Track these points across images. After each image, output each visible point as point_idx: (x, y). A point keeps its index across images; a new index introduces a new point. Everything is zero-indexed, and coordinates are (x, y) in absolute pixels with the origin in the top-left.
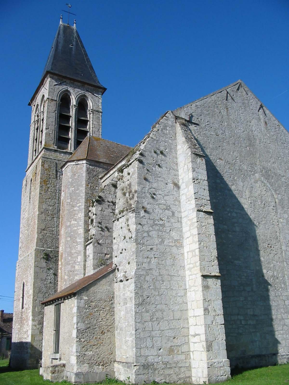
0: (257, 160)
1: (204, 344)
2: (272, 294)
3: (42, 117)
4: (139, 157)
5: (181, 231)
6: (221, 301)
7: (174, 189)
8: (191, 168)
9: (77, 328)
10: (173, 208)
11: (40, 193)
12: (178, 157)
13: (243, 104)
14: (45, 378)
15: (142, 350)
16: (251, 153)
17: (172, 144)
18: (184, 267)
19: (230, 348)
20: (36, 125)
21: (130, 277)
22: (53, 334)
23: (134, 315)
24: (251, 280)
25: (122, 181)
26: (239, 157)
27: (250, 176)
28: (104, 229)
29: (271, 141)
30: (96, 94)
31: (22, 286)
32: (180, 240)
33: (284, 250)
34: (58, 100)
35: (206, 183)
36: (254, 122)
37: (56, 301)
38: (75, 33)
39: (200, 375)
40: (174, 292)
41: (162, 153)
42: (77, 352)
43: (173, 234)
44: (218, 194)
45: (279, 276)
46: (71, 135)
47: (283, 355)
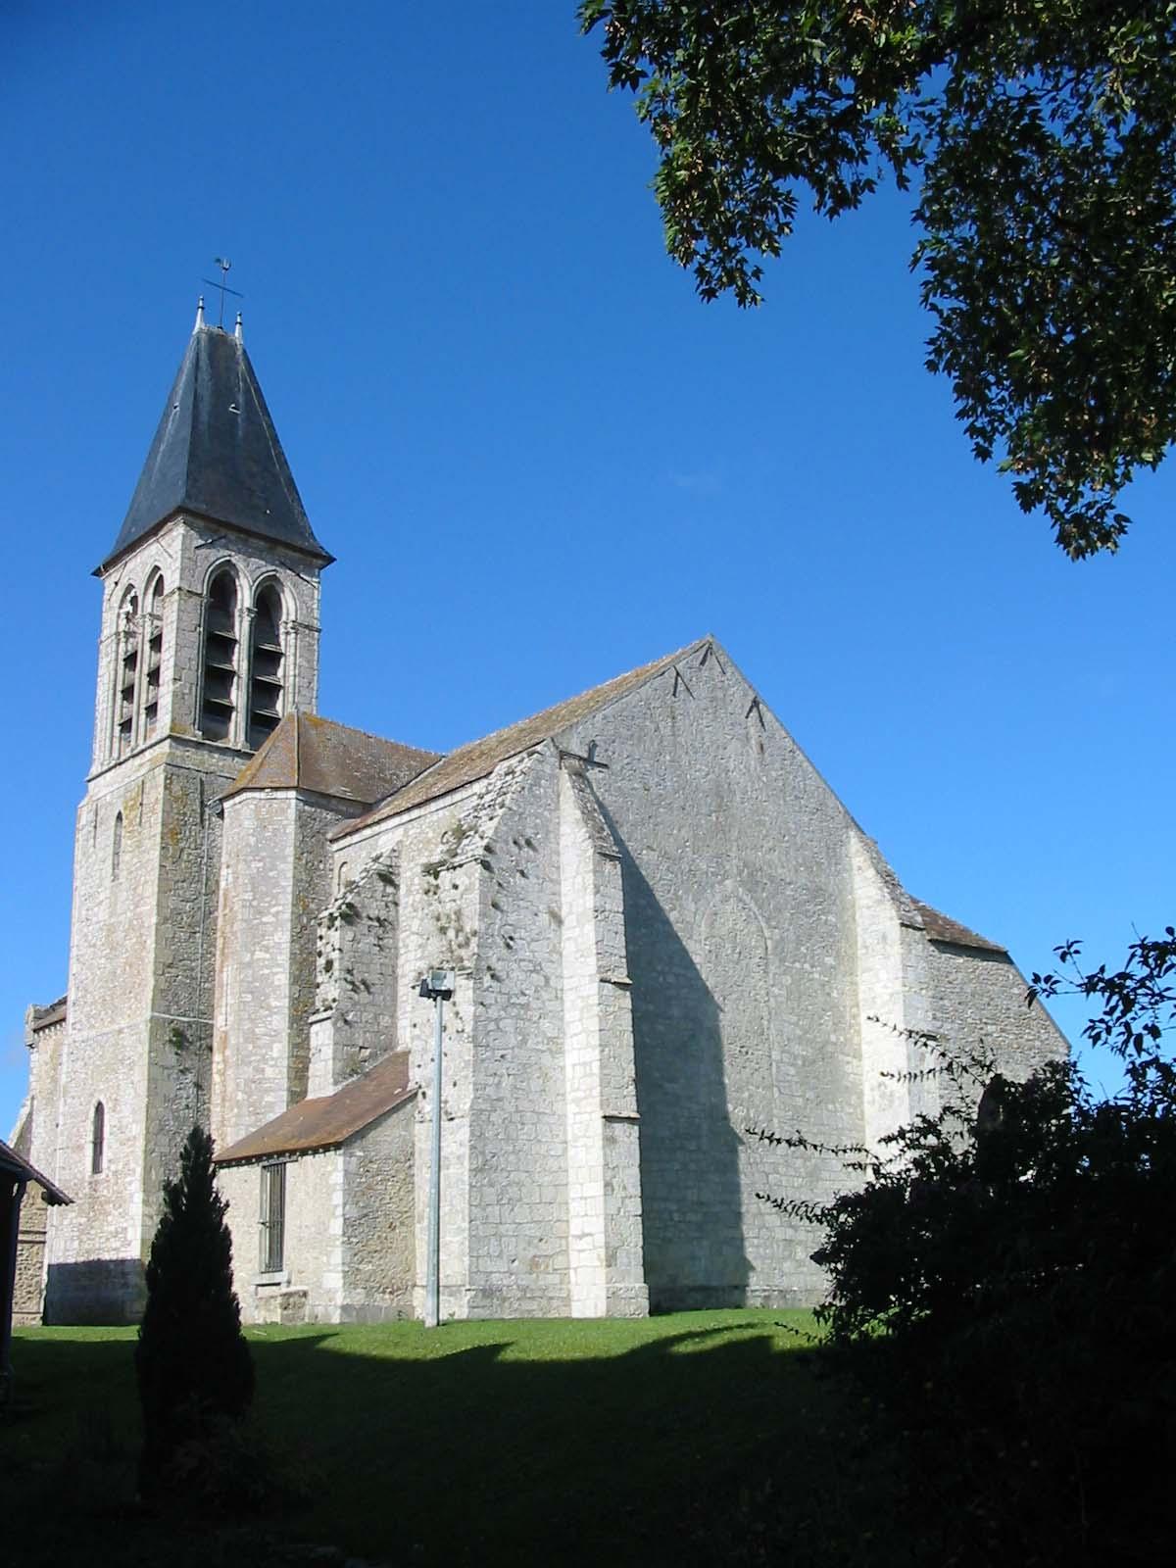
1: (602, 1252)
5: (562, 1019)
9: (344, 1215)
10: (548, 969)
12: (562, 851)
18: (563, 1095)
19: (650, 1269)
20: (122, 645)
21: (459, 1114)
27: (712, 886)
36: (734, 746)
38: (240, 361)
40: (544, 1147)
41: (529, 843)
42: (343, 1264)
43: (545, 1024)
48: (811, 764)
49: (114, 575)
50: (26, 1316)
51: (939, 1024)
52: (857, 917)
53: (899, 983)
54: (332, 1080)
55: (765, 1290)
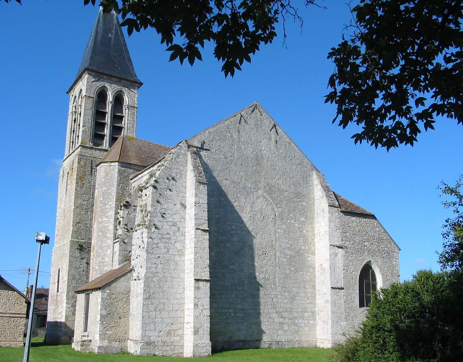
0: (262, 177)
1: (193, 329)
2: (262, 292)
3: (79, 110)
4: (154, 184)
5: (184, 243)
6: (209, 299)
7: (181, 208)
9: (101, 314)
10: (179, 225)
11: (76, 189)
12: (187, 181)
14: (76, 350)
15: (147, 332)
17: (183, 170)
18: (184, 271)
20: (74, 116)
22: (83, 317)
23: (142, 306)
24: (243, 281)
28: (129, 230)
30: (133, 89)
31: (58, 271)
32: (182, 250)
33: (278, 256)
37: (86, 292)
38: (115, 19)
39: (189, 352)
41: (173, 179)
45: (270, 278)
46: (107, 131)
47: (265, 342)
48: (298, 147)
49: (72, 93)
50: (18, 342)
51: (344, 242)
52: (315, 203)
53: (328, 227)
54: (118, 263)
55: (269, 341)
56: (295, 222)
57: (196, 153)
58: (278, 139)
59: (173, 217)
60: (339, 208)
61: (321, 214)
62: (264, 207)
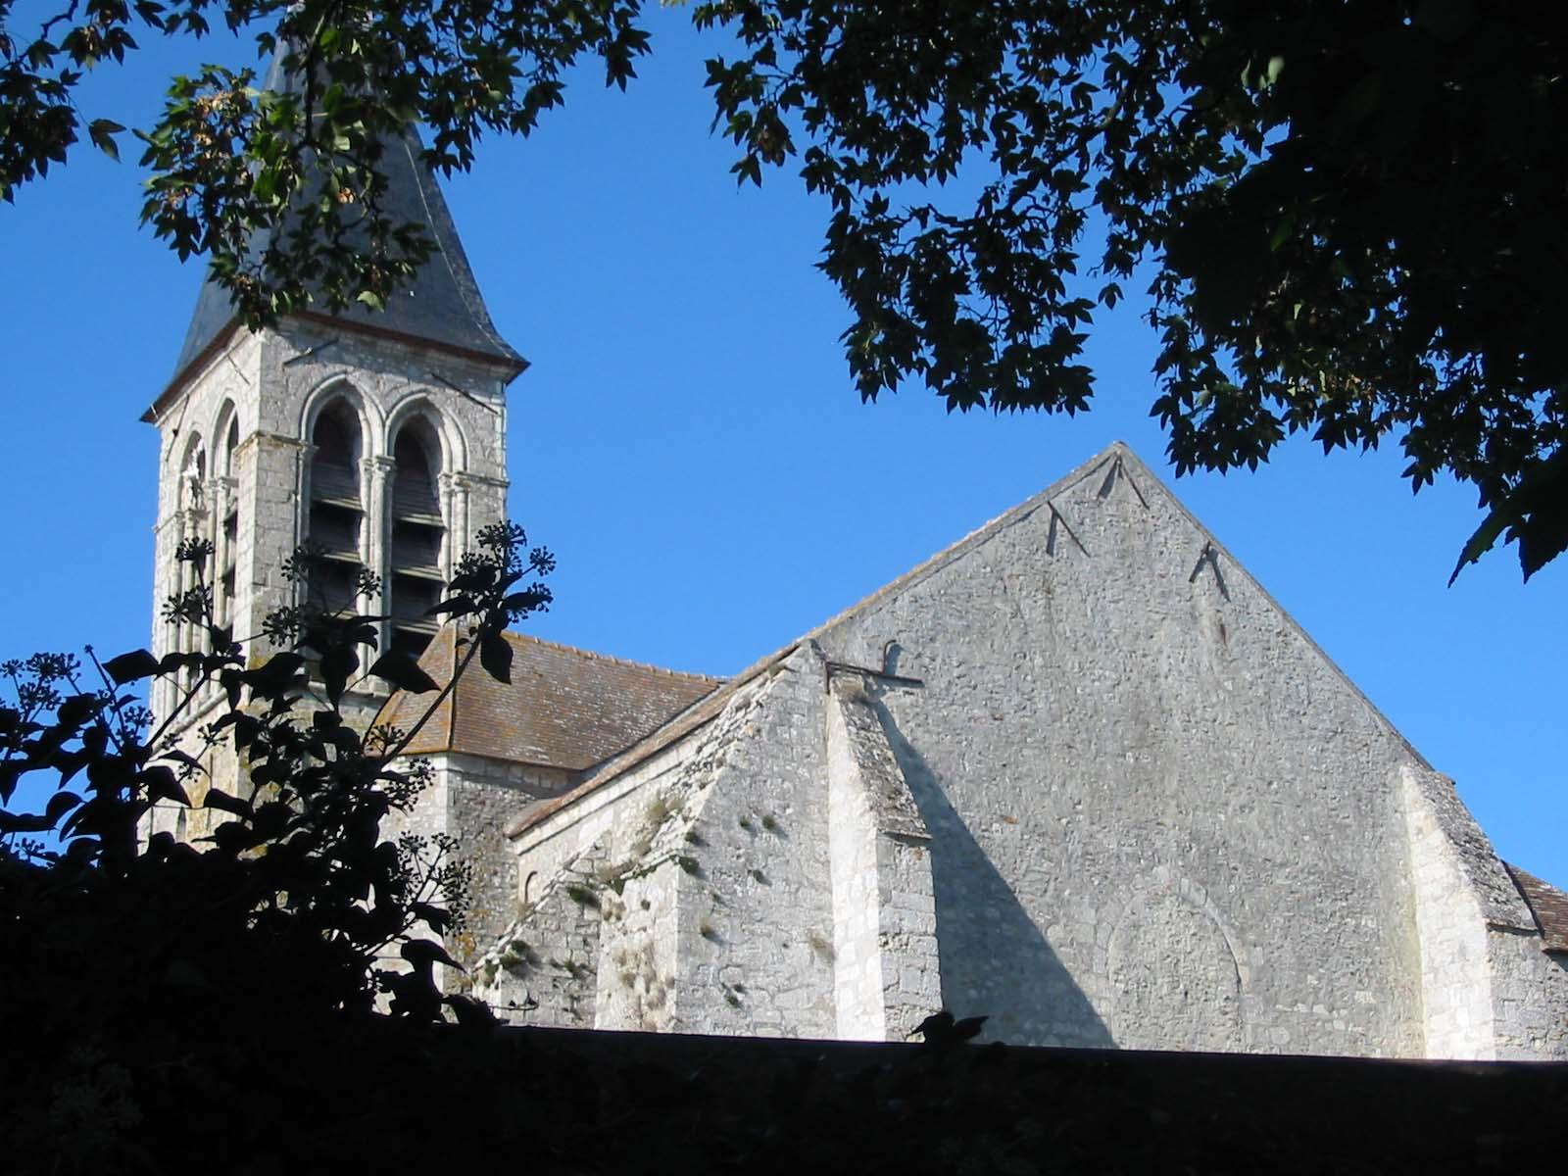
8: (877, 892)
12: (831, 833)
13: (1123, 557)
16: (1142, 776)
17: (810, 782)
25: (620, 924)
26: (1088, 799)
27: (1130, 878)
29: (1240, 710)
34: (303, 437)
35: (931, 944)
41: (769, 824)
44: (987, 968)
49: (171, 420)
53: (1488, 1030)
56: (1330, 1012)
57: (864, 702)
58: (1228, 619)
59: (777, 1003)
60: (1537, 938)
61: (1455, 968)
62: (1186, 944)
